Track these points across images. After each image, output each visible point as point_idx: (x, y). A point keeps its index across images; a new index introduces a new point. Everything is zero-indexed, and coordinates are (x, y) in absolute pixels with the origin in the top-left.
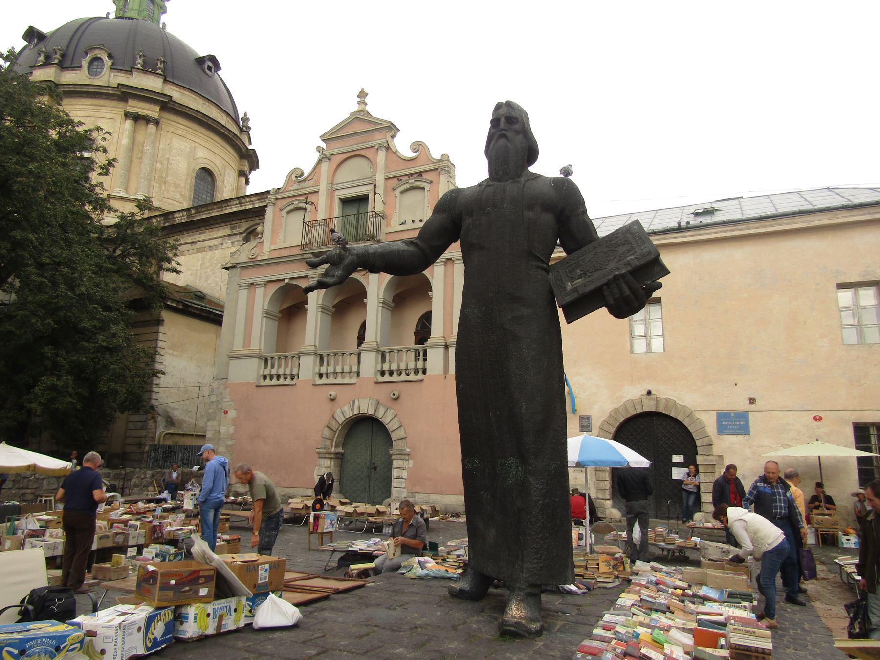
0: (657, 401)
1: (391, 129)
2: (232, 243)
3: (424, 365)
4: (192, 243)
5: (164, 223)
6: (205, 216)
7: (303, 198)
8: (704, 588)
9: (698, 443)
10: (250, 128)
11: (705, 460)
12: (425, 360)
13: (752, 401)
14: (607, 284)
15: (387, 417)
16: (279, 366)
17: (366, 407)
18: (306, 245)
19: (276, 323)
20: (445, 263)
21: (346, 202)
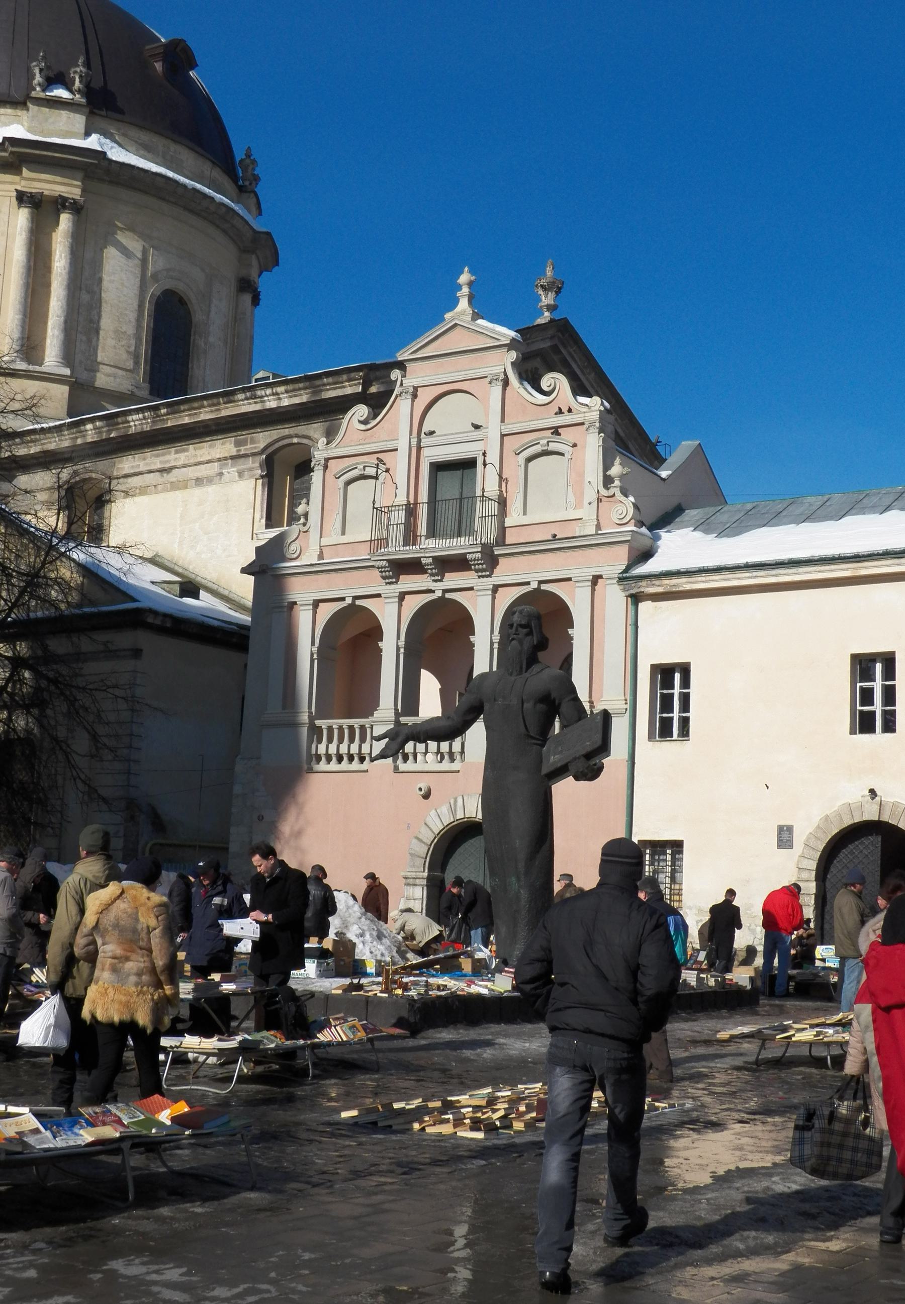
1: (474, 634)
2: (240, 474)
4: (162, 471)
5: (109, 432)
6: (187, 420)
7: (373, 459)
10: (257, 179)
21: (438, 468)
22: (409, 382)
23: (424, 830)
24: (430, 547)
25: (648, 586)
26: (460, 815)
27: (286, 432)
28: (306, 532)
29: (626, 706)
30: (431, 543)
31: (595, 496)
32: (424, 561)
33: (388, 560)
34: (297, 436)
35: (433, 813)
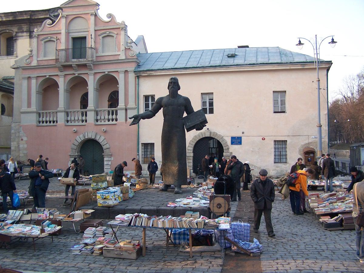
0: (210, 133)
3: (86, 118)
8: (238, 198)
9: (224, 148)
11: (226, 154)
12: (86, 116)
13: (243, 133)
14: (195, 125)
15: (101, 139)
16: (46, 117)
17: (91, 135)
18: (57, 60)
19: (42, 95)
20: (125, 72)
21: (74, 39)
22: (65, 14)
23: (75, 141)
24: (74, 62)
25: (143, 73)
26: (86, 137)
27: (4, 28)
28: (32, 56)
29: (136, 107)
30: (74, 60)
31: (125, 48)
32: (73, 65)
33: (76, 64)
34: (8, 30)
35: (78, 137)
